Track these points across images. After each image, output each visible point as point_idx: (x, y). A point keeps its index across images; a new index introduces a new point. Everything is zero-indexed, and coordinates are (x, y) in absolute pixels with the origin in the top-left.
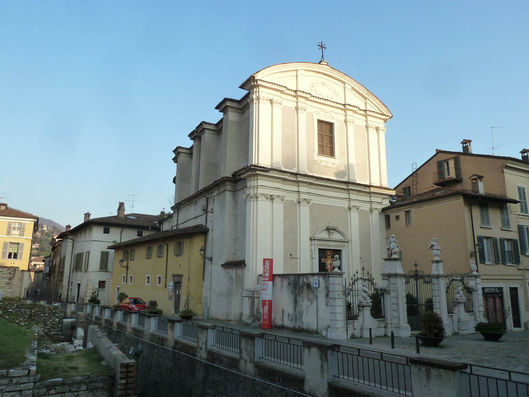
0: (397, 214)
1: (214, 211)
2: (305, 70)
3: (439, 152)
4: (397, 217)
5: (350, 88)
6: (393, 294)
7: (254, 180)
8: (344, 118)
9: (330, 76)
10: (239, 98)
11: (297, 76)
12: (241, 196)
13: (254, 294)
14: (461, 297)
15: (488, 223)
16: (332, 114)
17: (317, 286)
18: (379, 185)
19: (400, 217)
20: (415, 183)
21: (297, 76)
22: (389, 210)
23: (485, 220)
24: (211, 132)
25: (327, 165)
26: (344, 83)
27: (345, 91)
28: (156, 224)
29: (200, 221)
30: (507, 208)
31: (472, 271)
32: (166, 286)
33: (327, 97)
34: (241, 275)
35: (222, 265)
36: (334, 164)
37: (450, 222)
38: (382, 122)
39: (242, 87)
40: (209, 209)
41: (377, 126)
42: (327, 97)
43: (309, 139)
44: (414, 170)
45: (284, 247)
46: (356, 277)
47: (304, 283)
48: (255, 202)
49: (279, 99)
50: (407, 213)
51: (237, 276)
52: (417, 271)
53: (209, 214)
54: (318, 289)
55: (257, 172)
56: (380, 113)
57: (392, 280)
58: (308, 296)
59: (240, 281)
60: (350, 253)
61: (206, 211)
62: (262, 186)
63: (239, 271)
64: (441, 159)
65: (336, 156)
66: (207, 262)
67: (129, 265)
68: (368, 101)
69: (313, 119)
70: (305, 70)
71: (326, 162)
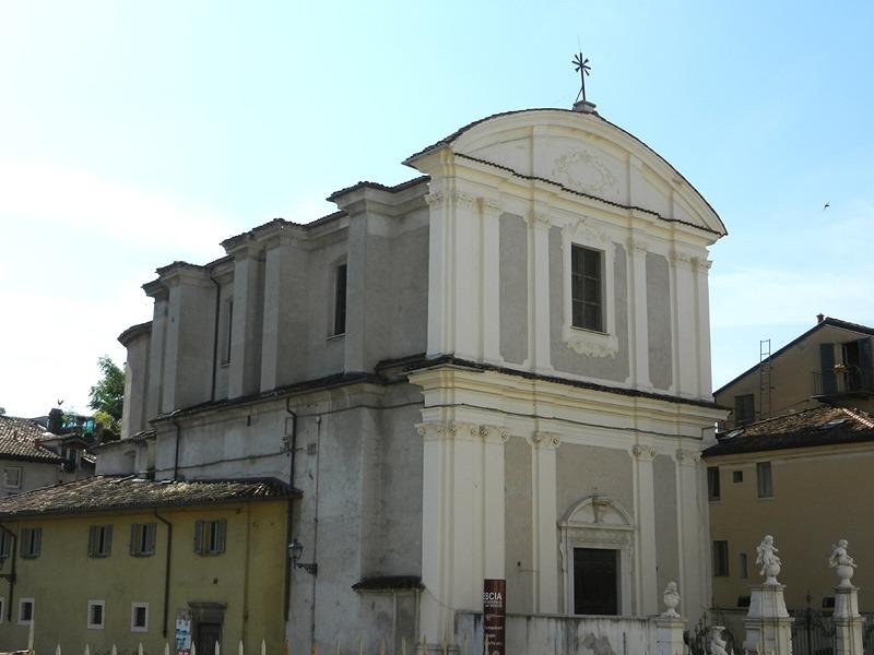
1: (322, 451)
4: (738, 476)
10: (391, 183)
12: (400, 422)
18: (694, 396)
27: (628, 174)
29: (278, 469)
32: (165, 632)
33: (570, 181)
35: (354, 587)
39: (410, 162)
40: (303, 442)
41: (693, 256)
42: (570, 181)
43: (548, 289)
44: (764, 358)
45: (507, 545)
46: (703, 627)
48: (448, 442)
50: (764, 468)
52: (809, 609)
53: (302, 457)
59: (407, 626)
60: (637, 557)
61: (291, 448)
62: (436, 388)
63: (407, 604)
65: (608, 332)
66: (300, 575)
67: (18, 571)
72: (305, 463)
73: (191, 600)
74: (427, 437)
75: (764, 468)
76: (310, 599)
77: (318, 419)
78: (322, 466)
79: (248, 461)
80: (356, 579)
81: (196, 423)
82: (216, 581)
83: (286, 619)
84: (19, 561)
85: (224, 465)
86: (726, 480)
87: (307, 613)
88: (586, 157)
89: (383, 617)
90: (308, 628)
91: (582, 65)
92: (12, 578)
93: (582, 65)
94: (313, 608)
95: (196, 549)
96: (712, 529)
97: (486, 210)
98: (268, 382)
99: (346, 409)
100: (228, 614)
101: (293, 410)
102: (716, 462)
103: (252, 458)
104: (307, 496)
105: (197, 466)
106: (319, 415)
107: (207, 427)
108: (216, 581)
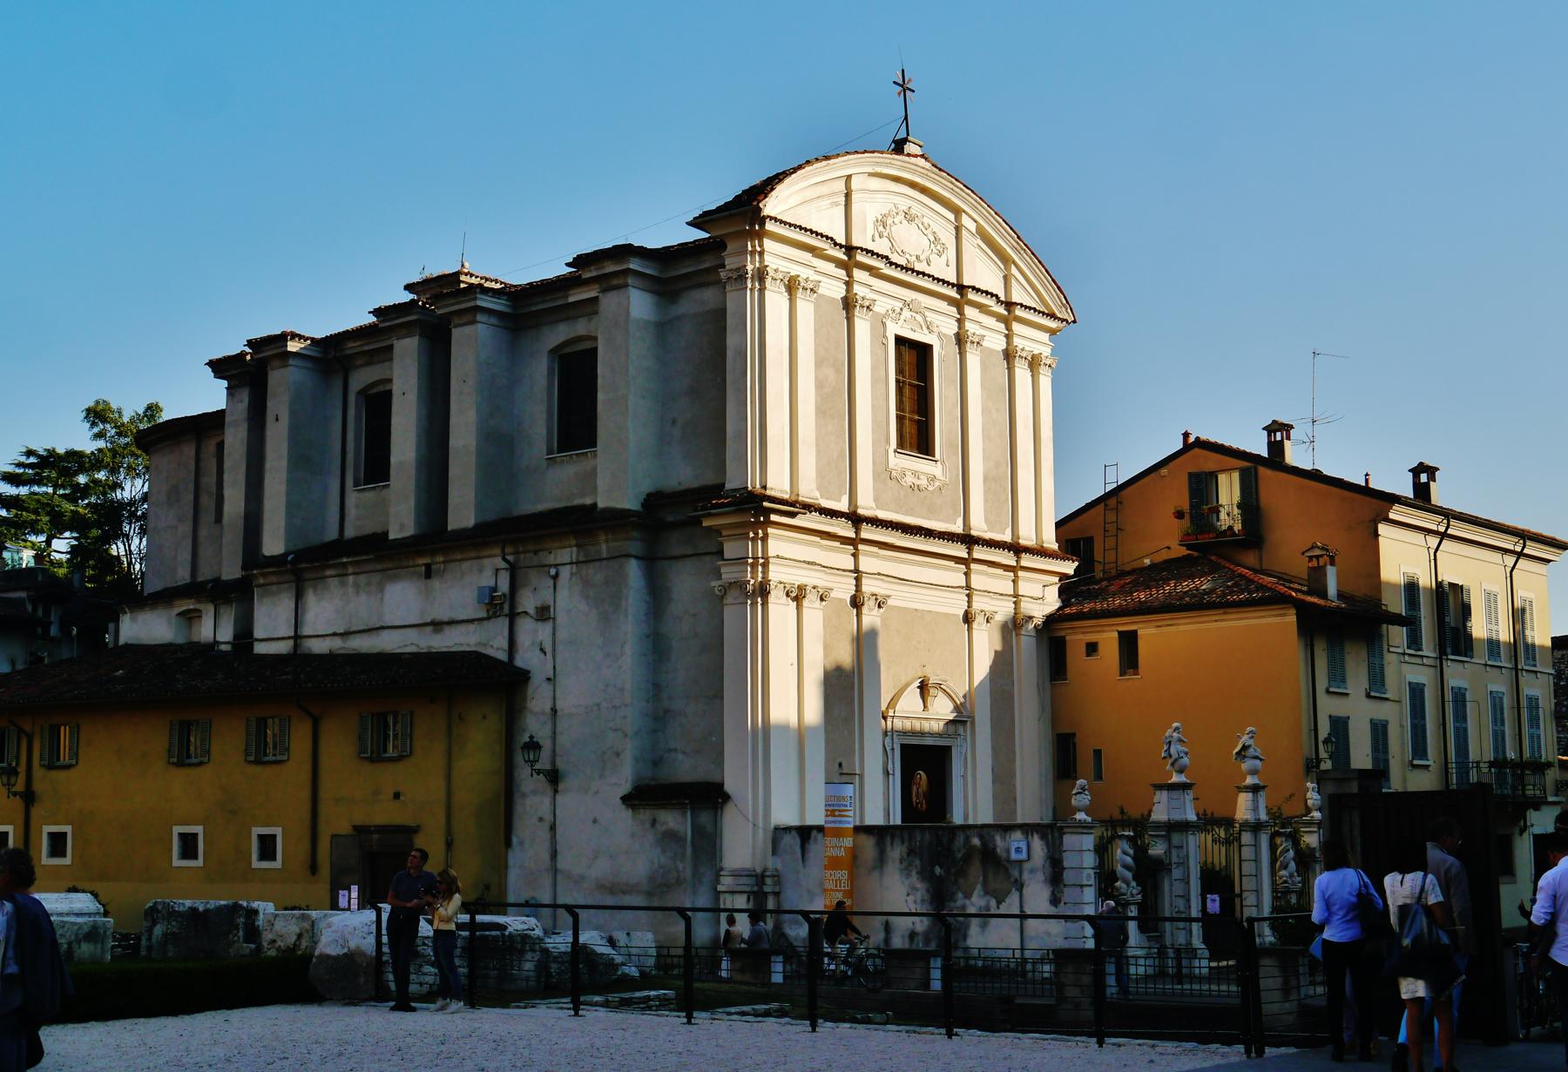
0: (1092, 638)
1: (561, 617)
2: (871, 174)
3: (1193, 446)
4: (1092, 648)
5: (972, 226)
6: (1177, 873)
7: (754, 540)
8: (954, 328)
9: (924, 190)
11: (848, 196)
12: (685, 583)
13: (764, 883)
14: (1291, 876)
15: (1343, 681)
16: (931, 316)
17: (1024, 856)
19: (1101, 648)
20: (1110, 527)
21: (848, 196)
22: (1068, 625)
23: (1338, 675)
24: (493, 320)
25: (917, 482)
26: (957, 212)
28: (20, 601)
29: (491, 640)
30: (1380, 636)
31: (1308, 810)
34: (710, 828)
36: (933, 478)
37: (1210, 661)
38: (1045, 337)
39: (696, 223)
47: (970, 851)
49: (814, 277)
50: (1129, 642)
51: (698, 831)
54: (1027, 866)
55: (774, 517)
56: (1042, 309)
57: (1176, 838)
58: (985, 884)
59: (707, 846)
63: (705, 818)
64: (1198, 461)
68: (1014, 270)
69: (885, 336)
70: (871, 174)
71: (916, 474)
72: (530, 633)
73: (358, 822)
75: (1129, 642)
76: (548, 817)
77: (553, 571)
78: (562, 634)
79: (429, 629)
80: (626, 788)
81: (328, 573)
82: (397, 796)
83: (508, 844)
84: (38, 772)
85: (385, 633)
87: (544, 834)
88: (909, 217)
89: (670, 837)
90: (546, 856)
91: (904, 87)
92: (29, 797)
93: (904, 87)
94: (553, 828)
95: (362, 750)
97: (800, 293)
98: (462, 513)
99: (601, 560)
100: (420, 841)
101: (510, 558)
103: (437, 625)
104: (537, 679)
105: (335, 634)
106: (556, 566)
108: (397, 796)
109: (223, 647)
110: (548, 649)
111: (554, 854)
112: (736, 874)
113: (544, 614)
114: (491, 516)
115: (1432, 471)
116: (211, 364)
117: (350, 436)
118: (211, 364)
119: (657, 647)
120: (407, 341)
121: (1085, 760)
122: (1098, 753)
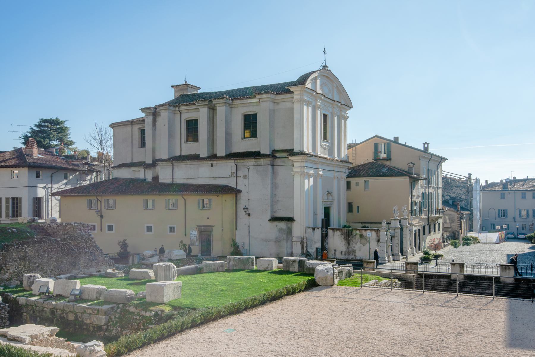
0: (357, 181)
4: (357, 184)
29: (232, 183)
32: (185, 235)
58: (360, 241)
59: (290, 232)
63: (289, 225)
72: (241, 180)
74: (295, 176)
80: (270, 218)
83: (236, 229)
86: (353, 185)
94: (249, 226)
95: (199, 208)
96: (347, 200)
98: (221, 151)
102: (349, 179)
107: (188, 166)
109: (149, 180)
110: (247, 185)
111: (249, 232)
112: (298, 238)
113: (245, 177)
114: (228, 153)
115: (428, 144)
116: (446, 159)
117: (183, 130)
118: (142, 109)
119: (274, 186)
120: (222, 108)
121: (355, 209)
122: (358, 207)
